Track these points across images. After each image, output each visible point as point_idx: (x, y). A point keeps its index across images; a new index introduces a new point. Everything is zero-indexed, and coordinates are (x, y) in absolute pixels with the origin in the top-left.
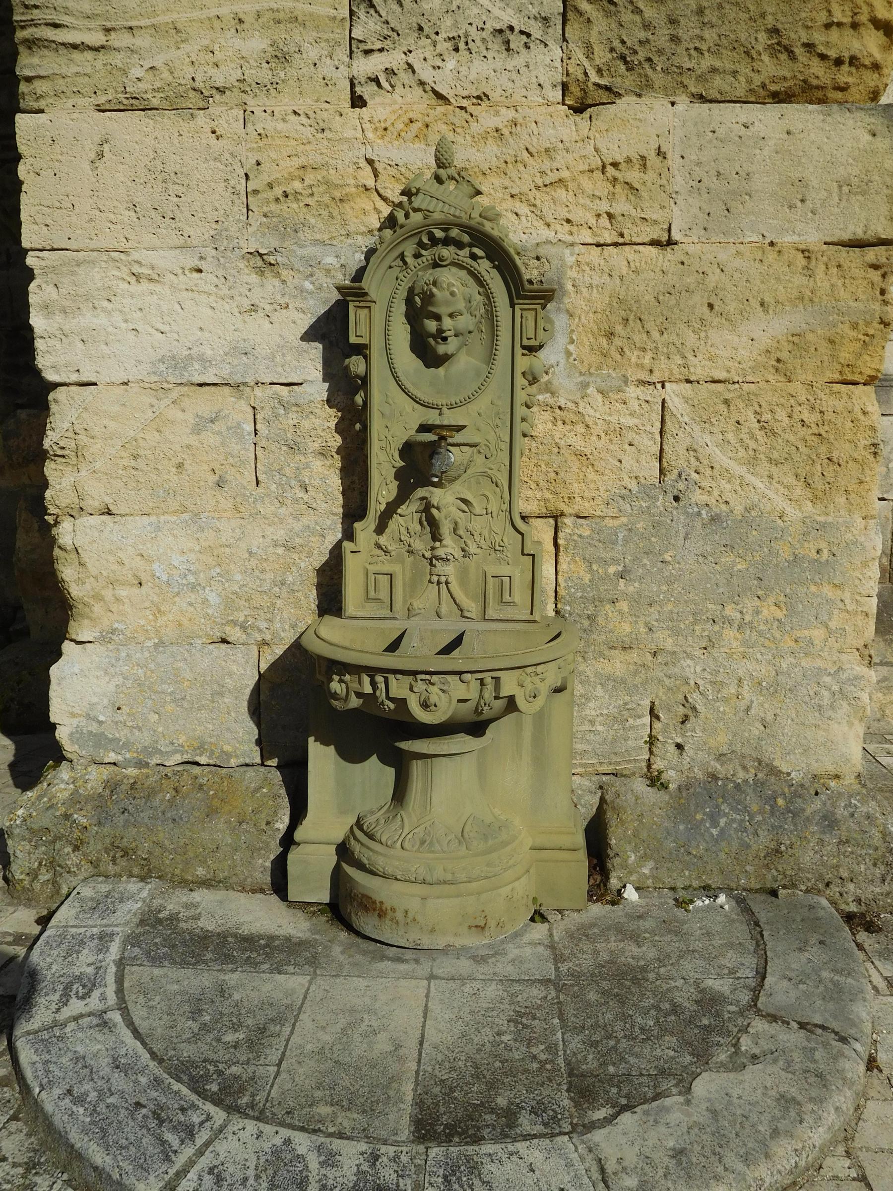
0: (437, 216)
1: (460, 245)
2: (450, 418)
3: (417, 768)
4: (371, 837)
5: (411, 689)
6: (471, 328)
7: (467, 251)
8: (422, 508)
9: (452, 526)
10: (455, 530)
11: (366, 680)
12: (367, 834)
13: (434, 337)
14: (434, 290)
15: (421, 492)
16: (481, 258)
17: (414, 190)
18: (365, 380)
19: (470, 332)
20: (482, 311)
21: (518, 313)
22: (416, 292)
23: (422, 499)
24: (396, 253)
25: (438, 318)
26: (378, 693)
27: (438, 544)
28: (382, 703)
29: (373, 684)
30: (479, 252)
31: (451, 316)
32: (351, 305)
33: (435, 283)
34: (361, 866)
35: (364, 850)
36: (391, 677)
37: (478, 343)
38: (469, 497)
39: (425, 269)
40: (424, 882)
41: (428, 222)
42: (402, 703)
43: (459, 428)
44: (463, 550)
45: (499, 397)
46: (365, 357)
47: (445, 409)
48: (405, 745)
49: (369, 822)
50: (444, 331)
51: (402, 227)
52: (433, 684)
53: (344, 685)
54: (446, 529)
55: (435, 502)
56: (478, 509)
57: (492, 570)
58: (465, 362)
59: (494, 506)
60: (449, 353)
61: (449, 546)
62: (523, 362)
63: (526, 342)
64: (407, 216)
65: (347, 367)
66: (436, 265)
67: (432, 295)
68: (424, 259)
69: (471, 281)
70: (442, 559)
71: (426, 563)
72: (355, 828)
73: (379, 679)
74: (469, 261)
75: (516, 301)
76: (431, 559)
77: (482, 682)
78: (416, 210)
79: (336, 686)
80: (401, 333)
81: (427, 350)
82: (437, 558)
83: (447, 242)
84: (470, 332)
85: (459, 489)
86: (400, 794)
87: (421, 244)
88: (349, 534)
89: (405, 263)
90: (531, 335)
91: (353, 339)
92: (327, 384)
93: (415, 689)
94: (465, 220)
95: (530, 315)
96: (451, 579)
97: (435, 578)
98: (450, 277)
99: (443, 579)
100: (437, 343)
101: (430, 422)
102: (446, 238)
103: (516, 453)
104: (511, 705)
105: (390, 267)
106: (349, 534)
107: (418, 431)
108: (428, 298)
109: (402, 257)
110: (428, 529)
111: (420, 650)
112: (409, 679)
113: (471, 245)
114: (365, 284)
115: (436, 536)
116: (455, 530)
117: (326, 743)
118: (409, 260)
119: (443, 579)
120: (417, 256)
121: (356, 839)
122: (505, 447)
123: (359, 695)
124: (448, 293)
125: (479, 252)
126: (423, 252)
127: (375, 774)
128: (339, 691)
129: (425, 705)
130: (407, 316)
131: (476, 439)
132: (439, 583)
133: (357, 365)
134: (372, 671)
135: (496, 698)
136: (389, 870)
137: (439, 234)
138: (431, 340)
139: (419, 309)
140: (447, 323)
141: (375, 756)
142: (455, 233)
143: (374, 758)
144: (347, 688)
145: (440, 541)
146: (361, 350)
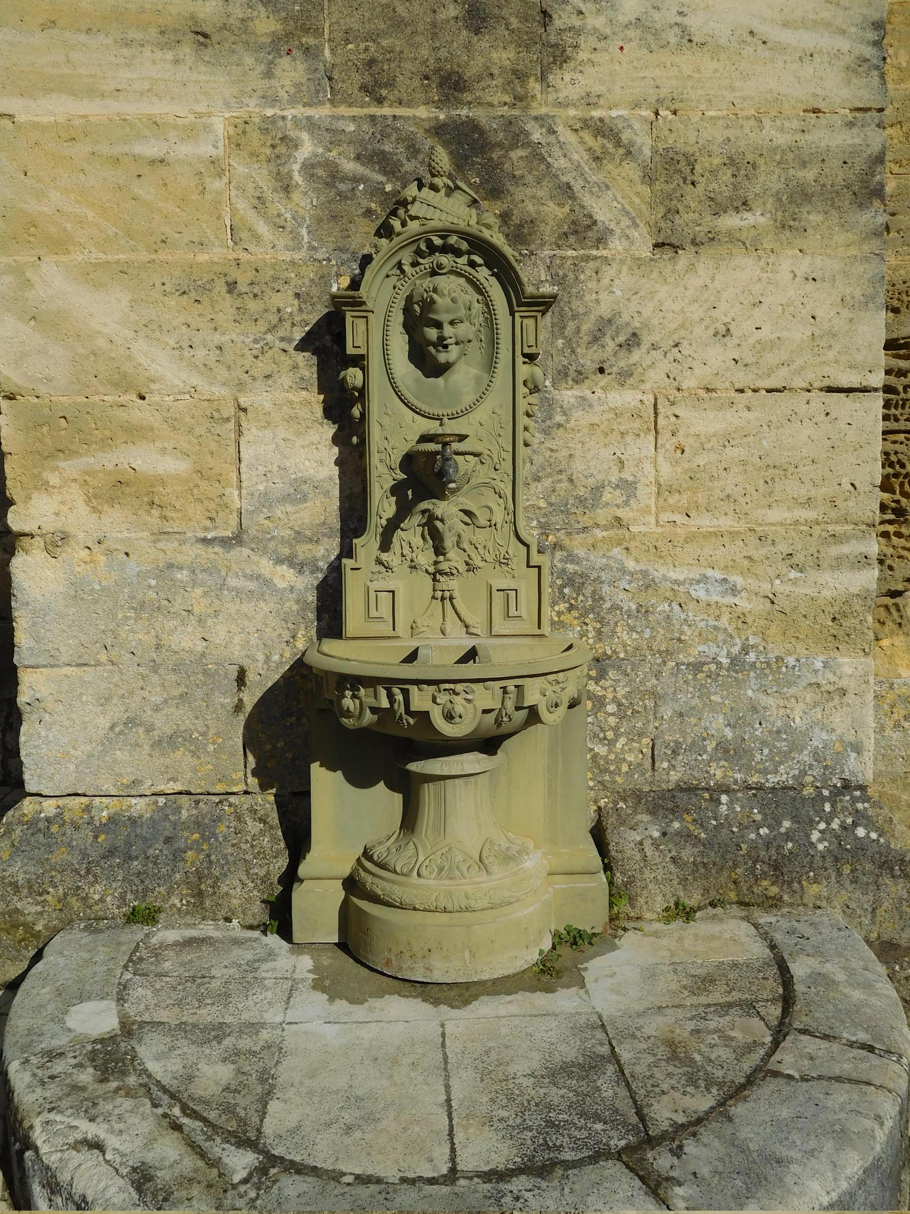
0: (432, 224)
1: (458, 253)
2: (451, 427)
3: (429, 792)
4: (383, 866)
5: (434, 700)
6: (471, 337)
7: (464, 260)
8: (424, 521)
9: (455, 539)
10: (458, 543)
11: (383, 693)
12: (377, 864)
13: (435, 345)
14: (435, 296)
15: (424, 505)
16: (480, 265)
17: (410, 199)
18: (363, 393)
19: (469, 341)
20: (481, 319)
21: (518, 320)
22: (415, 300)
23: (424, 512)
24: (394, 261)
25: (438, 325)
26: (396, 706)
27: (441, 558)
28: (401, 718)
29: (391, 696)
30: (479, 260)
31: (452, 323)
32: (348, 315)
33: (435, 290)
34: (375, 899)
35: (377, 880)
36: (413, 689)
37: (476, 351)
38: (473, 508)
39: (420, 278)
40: (445, 911)
41: (426, 228)
42: (424, 716)
43: (462, 438)
44: (467, 564)
45: (501, 406)
46: (363, 369)
47: (445, 420)
48: (413, 767)
49: (379, 852)
50: (445, 339)
51: (399, 234)
52: (457, 694)
53: (357, 701)
54: (449, 542)
55: (439, 512)
56: (482, 521)
57: (498, 583)
58: (465, 375)
59: (499, 516)
60: (451, 361)
61: (454, 558)
62: (524, 370)
63: (527, 350)
64: (404, 224)
65: (344, 379)
66: (433, 273)
67: (433, 302)
68: (422, 267)
69: (470, 289)
70: (446, 574)
71: (429, 579)
72: (363, 860)
73: (396, 691)
74: (468, 269)
75: (516, 308)
76: (434, 574)
77: (504, 689)
78: (413, 218)
79: (348, 702)
80: (399, 344)
81: (427, 361)
82: (441, 573)
83: (446, 249)
84: (469, 341)
85: (464, 500)
86: (409, 820)
87: (419, 253)
88: (347, 551)
89: (403, 272)
90: (532, 343)
91: (350, 350)
92: (322, 397)
93: (438, 701)
94: (462, 226)
95: (530, 322)
96: (456, 594)
97: (439, 594)
98: (449, 284)
99: (447, 594)
100: (438, 351)
101: (432, 432)
102: (444, 245)
103: (519, 462)
104: (533, 716)
105: (388, 276)
106: (347, 551)
107: (419, 442)
108: (428, 305)
109: (399, 265)
110: (431, 542)
111: (440, 657)
112: (433, 688)
113: (469, 253)
114: (363, 291)
115: (439, 550)
116: (458, 543)
117: (332, 768)
118: (407, 268)
119: (447, 594)
120: (414, 264)
121: (366, 870)
122: (508, 457)
123: (374, 710)
124: (449, 300)
125: (479, 260)
126: (421, 261)
127: (383, 801)
128: (352, 708)
129: (449, 717)
130: (405, 326)
131: (478, 448)
132: (443, 599)
133: (353, 376)
134: (389, 683)
135: (518, 708)
136: (407, 899)
137: (438, 241)
138: (431, 349)
139: (418, 318)
140: (448, 330)
141: (382, 783)
142: (453, 240)
143: (381, 784)
144: (361, 704)
145: (444, 554)
146: (359, 361)
